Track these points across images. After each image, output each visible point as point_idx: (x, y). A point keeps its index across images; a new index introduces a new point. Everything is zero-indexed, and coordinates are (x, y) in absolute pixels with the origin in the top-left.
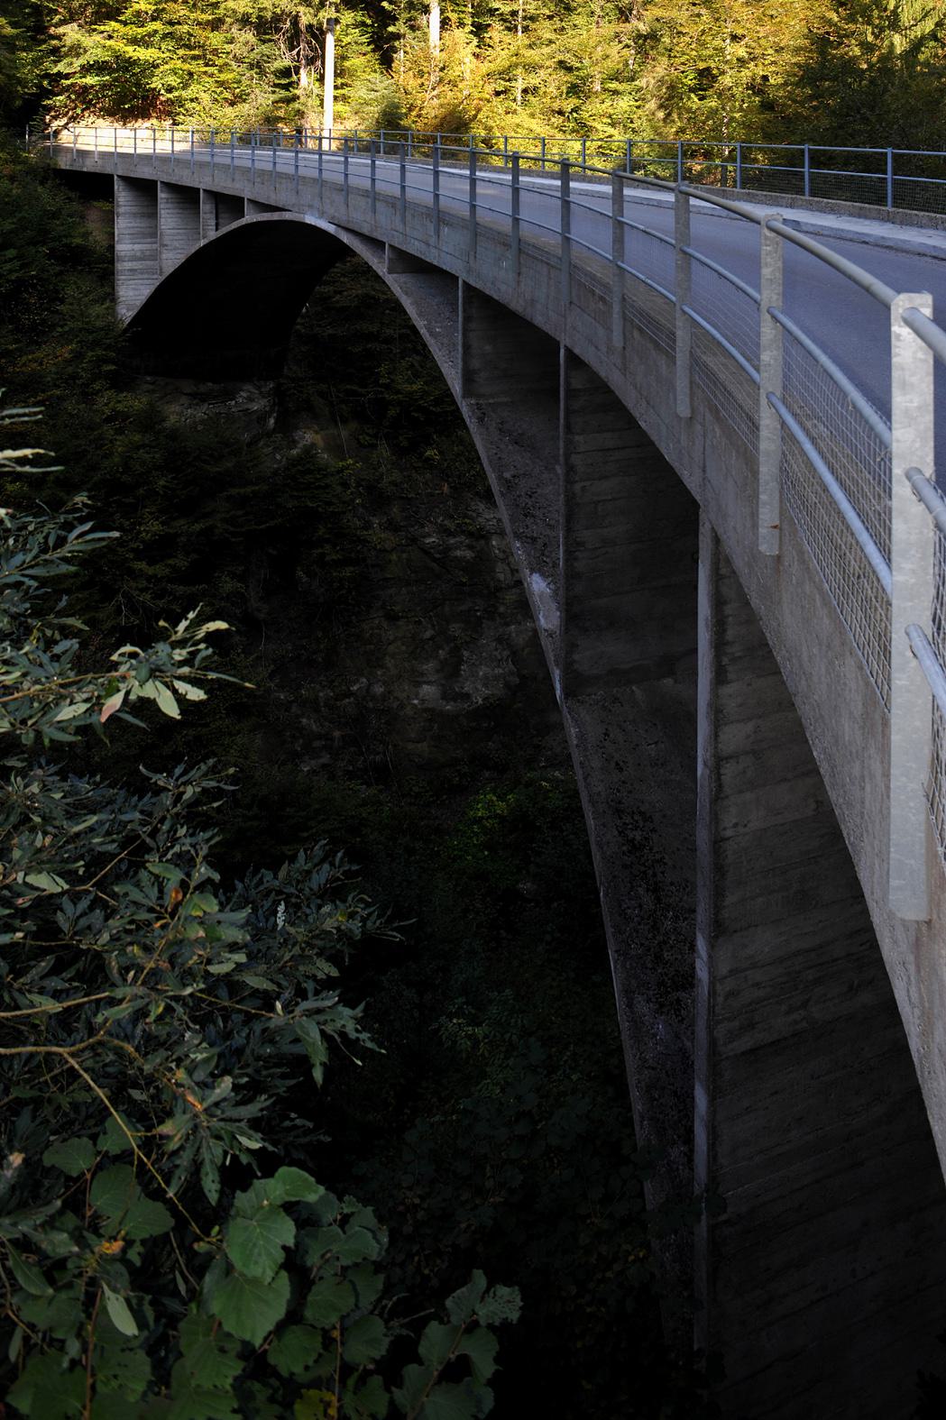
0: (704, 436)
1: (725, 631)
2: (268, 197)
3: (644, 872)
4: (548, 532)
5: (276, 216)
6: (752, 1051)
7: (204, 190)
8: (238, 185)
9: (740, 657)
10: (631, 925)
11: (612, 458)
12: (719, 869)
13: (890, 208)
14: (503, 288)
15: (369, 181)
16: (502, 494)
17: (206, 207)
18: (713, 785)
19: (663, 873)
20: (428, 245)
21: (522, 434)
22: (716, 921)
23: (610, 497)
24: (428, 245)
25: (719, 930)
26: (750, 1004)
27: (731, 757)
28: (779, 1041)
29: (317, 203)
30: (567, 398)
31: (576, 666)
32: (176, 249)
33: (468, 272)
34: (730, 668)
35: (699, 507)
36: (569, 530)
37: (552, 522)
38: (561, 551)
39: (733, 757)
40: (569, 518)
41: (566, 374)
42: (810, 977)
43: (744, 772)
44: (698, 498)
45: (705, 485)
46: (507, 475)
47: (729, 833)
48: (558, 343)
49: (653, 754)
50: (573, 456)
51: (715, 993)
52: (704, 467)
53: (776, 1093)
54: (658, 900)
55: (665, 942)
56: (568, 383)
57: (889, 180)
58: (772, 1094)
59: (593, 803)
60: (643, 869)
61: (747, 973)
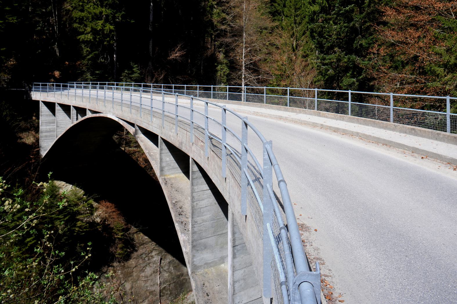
0: (230, 183)
2: (95, 108)
5: (97, 115)
7: (73, 106)
9: (240, 250)
11: (205, 193)
14: (173, 138)
16: (172, 208)
17: (73, 112)
18: (232, 290)
23: (205, 206)
27: (237, 281)
29: (112, 110)
30: (192, 174)
31: (195, 263)
34: (237, 253)
35: (228, 204)
36: (192, 218)
37: (188, 216)
38: (190, 225)
44: (228, 202)
45: (230, 198)
48: (189, 156)
56: (192, 170)
57: (288, 98)
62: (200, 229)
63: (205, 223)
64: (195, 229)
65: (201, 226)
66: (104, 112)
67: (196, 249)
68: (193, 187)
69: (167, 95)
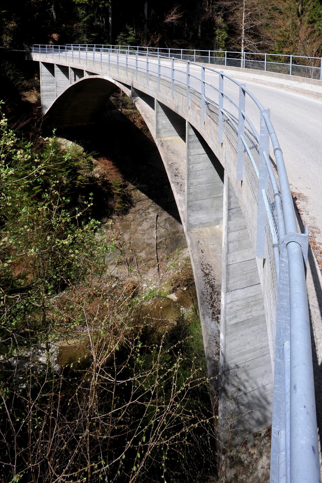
1: (231, 205)
3: (209, 282)
4: (182, 181)
5: (94, 77)
6: (236, 324)
8: (82, 65)
9: (235, 213)
10: (205, 297)
12: (228, 273)
14: (169, 102)
17: (71, 73)
19: (214, 282)
20: (145, 87)
21: (174, 150)
22: (227, 288)
24: (145, 87)
25: (228, 291)
26: (236, 311)
27: (232, 242)
28: (243, 321)
29: (108, 72)
30: (188, 138)
31: (190, 222)
33: (158, 97)
34: (232, 216)
36: (188, 180)
39: (233, 242)
40: (189, 175)
41: (188, 130)
42: (253, 304)
43: (235, 246)
44: (224, 167)
46: (169, 163)
47: (230, 263)
48: (185, 120)
49: (212, 248)
50: (190, 156)
51: (226, 308)
52: (226, 157)
53: (242, 335)
54: (213, 290)
55: (214, 301)
56: (188, 133)
57: (291, 66)
58: (241, 336)
59: (195, 262)
60: (208, 281)
61: (235, 302)
63: (200, 186)
64: (190, 190)
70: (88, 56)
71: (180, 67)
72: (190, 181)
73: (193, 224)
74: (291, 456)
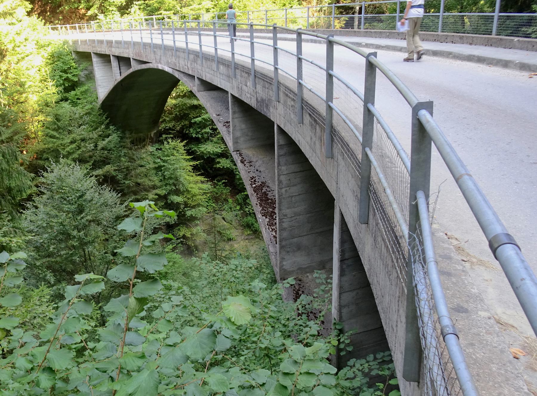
5: (144, 66)
13: (440, 33)
15: (161, 40)
17: (114, 63)
31: (284, 267)
32: (104, 87)
35: (334, 200)
44: (334, 196)
48: (274, 123)
62: (291, 225)
63: (298, 217)
64: (283, 224)
65: (292, 221)
66: (154, 62)
67: (286, 250)
68: (280, 167)
69: (483, 207)
70: (164, 38)
71: (344, 114)
72: (283, 211)
73: (289, 270)
74: (286, 73)
